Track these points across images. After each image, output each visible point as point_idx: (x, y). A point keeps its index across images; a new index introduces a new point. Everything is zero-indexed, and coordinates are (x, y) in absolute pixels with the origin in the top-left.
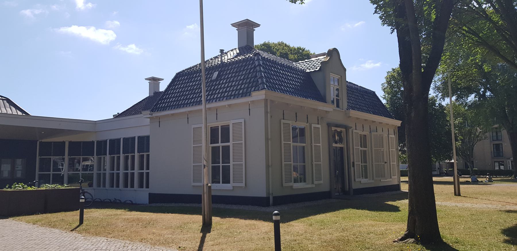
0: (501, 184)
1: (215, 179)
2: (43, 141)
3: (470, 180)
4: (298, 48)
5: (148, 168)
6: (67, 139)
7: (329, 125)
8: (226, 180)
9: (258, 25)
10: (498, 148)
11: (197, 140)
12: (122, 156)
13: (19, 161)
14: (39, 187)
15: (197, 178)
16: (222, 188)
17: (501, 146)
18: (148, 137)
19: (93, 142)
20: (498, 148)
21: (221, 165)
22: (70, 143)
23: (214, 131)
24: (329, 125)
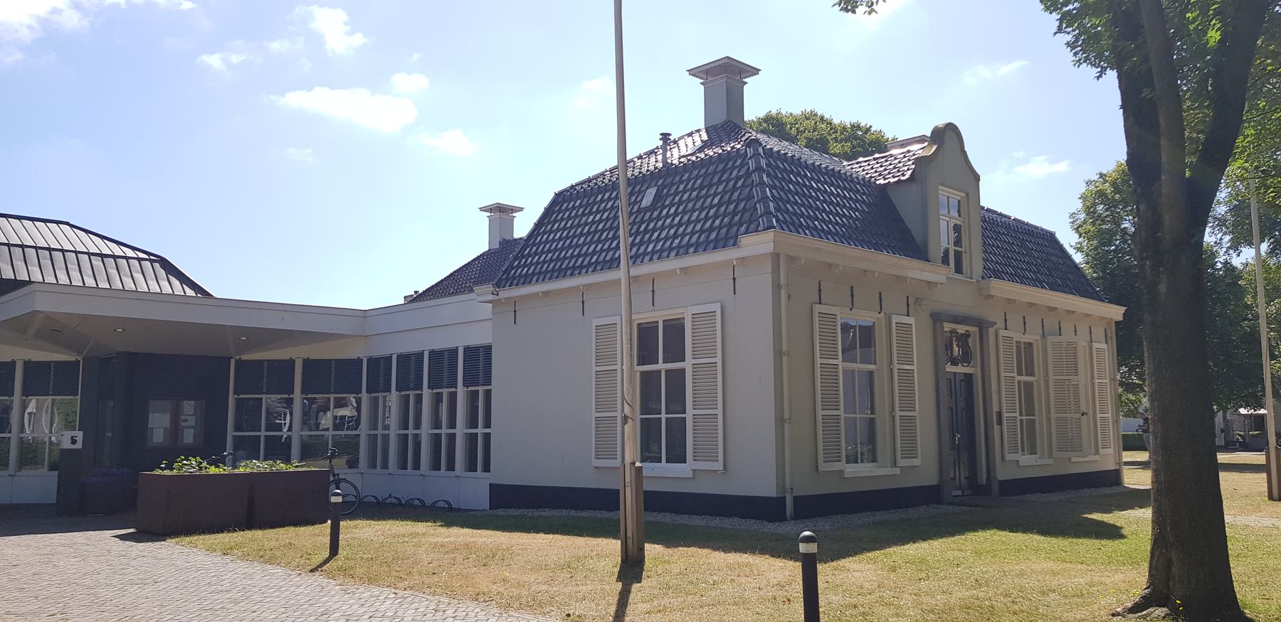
1: (649, 452)
2: (244, 357)
6: (298, 353)
9: (755, 71)
12: (461, 391)
15: (606, 446)
16: (665, 475)
18: (488, 349)
21: (664, 416)
22: (308, 363)
23: (646, 334)
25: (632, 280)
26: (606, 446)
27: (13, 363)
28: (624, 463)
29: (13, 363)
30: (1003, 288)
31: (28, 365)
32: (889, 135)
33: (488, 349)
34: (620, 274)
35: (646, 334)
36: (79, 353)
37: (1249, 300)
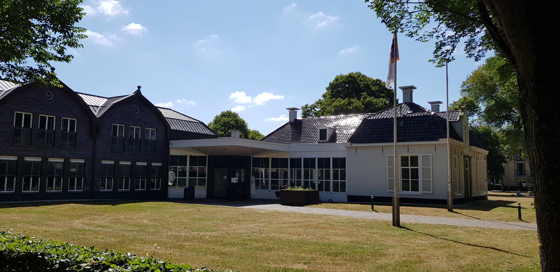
0: (9, 213)
1: (405, 188)
2: (255, 157)
3: (515, 194)
4: (377, 80)
5: (312, 178)
6: (270, 156)
7: (465, 156)
8: (417, 190)
9: (415, 88)
10: (521, 167)
11: (391, 164)
12: (303, 169)
13: (242, 170)
14: (305, 188)
15: (391, 187)
16: (410, 193)
17: (523, 166)
18: (345, 158)
19: (287, 159)
20: (521, 167)
21: (410, 180)
22: (272, 158)
23: (404, 160)
24: (465, 156)
25: (396, 145)
26: (391, 187)
27: (186, 156)
28: (397, 192)
29: (186, 156)
30: (475, 148)
31: (191, 157)
32: (398, 62)
33: (345, 158)
34: (394, 144)
35: (404, 160)
36: (206, 153)
37: (533, 111)
